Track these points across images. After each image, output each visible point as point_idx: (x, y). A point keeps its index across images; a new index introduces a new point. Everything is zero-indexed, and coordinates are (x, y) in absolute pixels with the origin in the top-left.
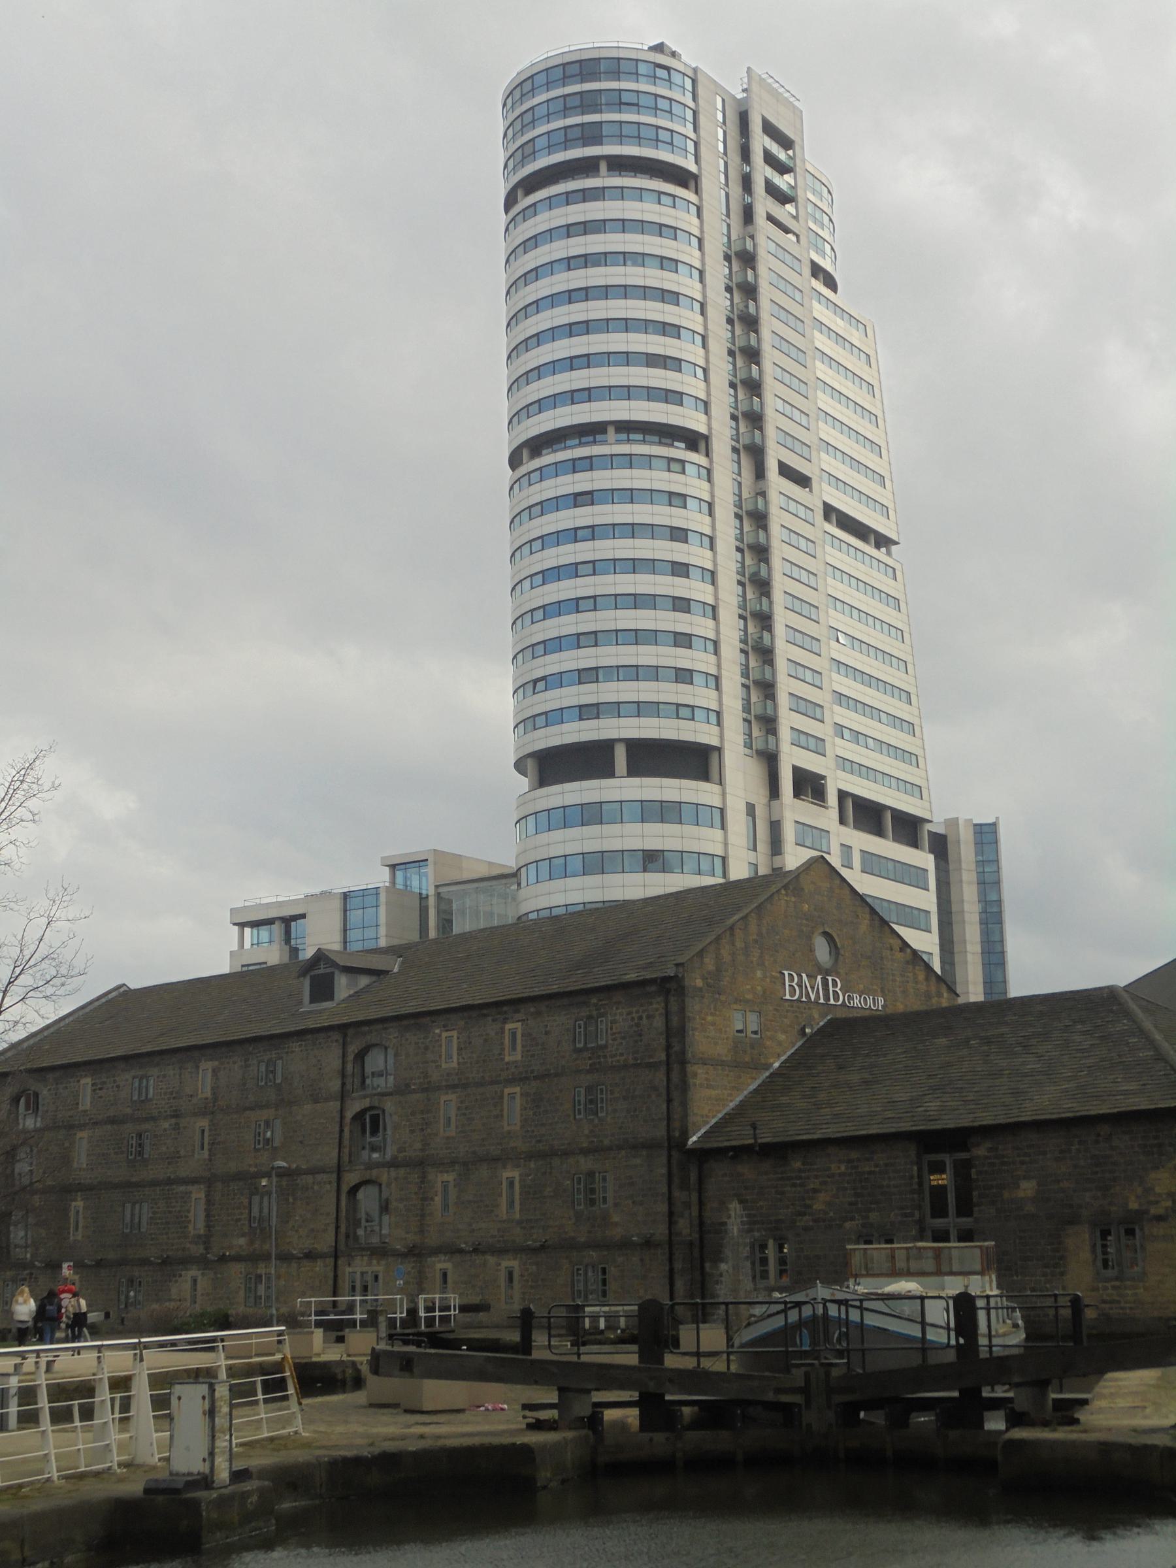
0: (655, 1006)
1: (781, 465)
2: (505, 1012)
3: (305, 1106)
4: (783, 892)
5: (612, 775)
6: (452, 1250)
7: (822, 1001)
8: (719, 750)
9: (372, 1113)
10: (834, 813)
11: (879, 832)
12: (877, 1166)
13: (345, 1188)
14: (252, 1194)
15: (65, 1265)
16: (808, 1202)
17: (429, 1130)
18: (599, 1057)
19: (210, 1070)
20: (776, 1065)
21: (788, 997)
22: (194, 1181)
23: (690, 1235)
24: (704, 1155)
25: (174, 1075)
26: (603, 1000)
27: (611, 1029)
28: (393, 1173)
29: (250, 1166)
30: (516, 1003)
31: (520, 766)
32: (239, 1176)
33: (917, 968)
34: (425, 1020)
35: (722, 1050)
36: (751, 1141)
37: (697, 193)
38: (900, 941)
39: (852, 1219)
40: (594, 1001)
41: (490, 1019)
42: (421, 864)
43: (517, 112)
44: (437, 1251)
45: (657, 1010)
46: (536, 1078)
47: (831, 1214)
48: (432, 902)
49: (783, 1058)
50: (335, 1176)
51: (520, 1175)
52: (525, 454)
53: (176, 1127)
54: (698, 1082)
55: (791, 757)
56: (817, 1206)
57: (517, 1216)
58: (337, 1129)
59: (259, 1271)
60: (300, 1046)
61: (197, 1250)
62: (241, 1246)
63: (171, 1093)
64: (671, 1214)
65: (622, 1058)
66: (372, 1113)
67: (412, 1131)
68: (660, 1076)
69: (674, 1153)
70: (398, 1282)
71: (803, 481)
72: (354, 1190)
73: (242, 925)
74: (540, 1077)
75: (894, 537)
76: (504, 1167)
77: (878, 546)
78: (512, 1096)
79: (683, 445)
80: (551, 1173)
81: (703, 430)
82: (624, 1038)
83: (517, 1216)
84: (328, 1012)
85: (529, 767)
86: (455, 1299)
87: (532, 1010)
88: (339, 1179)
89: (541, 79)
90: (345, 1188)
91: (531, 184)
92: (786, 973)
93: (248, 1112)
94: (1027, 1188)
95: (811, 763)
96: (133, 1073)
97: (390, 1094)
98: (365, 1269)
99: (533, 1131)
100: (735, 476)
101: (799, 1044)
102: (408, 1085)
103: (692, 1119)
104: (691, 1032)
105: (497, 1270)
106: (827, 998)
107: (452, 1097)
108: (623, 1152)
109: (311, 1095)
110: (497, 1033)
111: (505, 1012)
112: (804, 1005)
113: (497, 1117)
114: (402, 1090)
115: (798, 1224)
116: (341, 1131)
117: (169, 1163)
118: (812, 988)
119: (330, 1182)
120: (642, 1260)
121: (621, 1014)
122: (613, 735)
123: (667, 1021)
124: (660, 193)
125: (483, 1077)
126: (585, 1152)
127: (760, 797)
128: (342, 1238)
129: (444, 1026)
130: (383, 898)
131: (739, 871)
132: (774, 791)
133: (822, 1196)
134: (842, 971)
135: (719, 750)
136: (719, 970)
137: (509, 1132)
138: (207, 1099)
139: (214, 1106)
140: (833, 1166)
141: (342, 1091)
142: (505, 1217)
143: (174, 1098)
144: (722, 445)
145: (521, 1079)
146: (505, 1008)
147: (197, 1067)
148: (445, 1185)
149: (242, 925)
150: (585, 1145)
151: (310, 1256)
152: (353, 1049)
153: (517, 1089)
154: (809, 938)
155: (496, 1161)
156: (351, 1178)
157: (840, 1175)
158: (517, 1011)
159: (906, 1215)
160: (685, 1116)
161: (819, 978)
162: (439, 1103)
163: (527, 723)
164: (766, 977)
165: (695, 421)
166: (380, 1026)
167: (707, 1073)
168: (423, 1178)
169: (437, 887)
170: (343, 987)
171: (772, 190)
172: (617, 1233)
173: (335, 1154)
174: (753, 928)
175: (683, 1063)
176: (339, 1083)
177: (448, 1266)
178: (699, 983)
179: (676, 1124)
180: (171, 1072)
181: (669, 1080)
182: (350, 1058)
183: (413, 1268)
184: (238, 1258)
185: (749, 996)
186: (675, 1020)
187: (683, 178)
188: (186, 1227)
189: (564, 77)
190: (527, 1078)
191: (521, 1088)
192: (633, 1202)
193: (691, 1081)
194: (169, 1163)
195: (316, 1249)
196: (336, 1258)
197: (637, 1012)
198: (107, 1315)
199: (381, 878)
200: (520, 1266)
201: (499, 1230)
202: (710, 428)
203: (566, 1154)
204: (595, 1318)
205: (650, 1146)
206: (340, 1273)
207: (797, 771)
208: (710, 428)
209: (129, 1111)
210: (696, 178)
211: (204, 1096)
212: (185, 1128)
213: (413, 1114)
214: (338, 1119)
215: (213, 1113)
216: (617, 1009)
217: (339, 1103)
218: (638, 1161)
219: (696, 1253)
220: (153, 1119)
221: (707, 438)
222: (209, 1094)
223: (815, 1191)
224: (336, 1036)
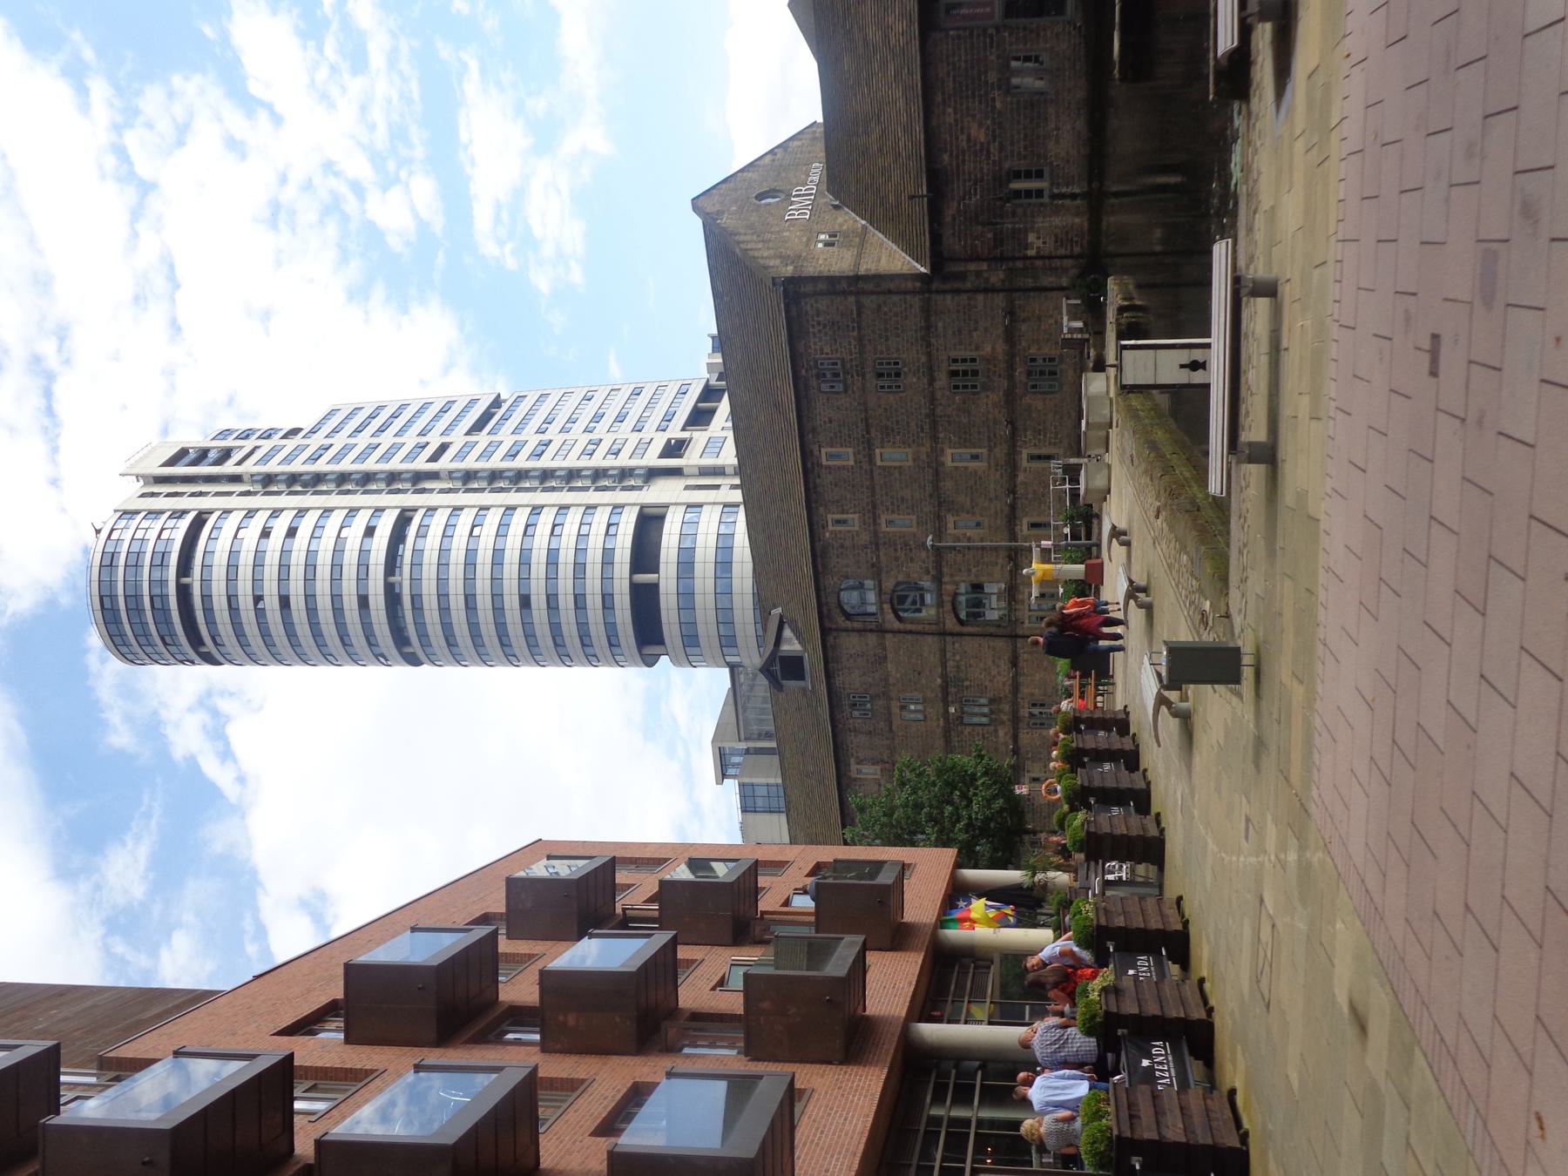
0: (809, 308)
1: (429, 460)
7: (812, 197)
8: (643, 507)
9: (896, 602)
10: (696, 435)
12: (948, 74)
14: (962, 723)
16: (978, 147)
18: (852, 366)
21: (807, 217)
24: (938, 259)
27: (827, 354)
28: (946, 579)
30: (806, 454)
36: (925, 199)
37: (212, 513)
39: (994, 100)
41: (818, 481)
43: (139, 650)
45: (812, 306)
46: (868, 433)
47: (989, 122)
48: (752, 744)
49: (858, 218)
50: (948, 638)
51: (950, 448)
52: (408, 650)
55: (652, 459)
56: (982, 138)
57: (984, 451)
58: (909, 637)
59: (1027, 715)
60: (838, 676)
62: (1006, 734)
64: (986, 290)
66: (896, 602)
67: (912, 560)
68: (868, 301)
69: (934, 286)
75: (494, 396)
76: (943, 464)
77: (499, 407)
79: (401, 546)
80: (949, 416)
82: (836, 340)
83: (984, 451)
84: (813, 662)
87: (810, 436)
88: (952, 634)
89: (113, 627)
90: (958, 628)
97: (880, 584)
101: (847, 209)
102: (873, 565)
103: (905, 270)
106: (811, 194)
107: (883, 519)
108: (933, 341)
110: (830, 473)
111: (813, 464)
113: (900, 474)
114: (876, 571)
115: (997, 158)
119: (954, 643)
120: (1024, 321)
121: (815, 344)
122: (626, 583)
123: (822, 293)
124: (209, 538)
125: (867, 488)
126: (932, 381)
129: (823, 528)
130: (746, 780)
131: (737, 496)
132: (676, 472)
133: (973, 132)
134: (788, 187)
136: (780, 257)
137: (914, 460)
138: (882, 770)
141: (878, 631)
142: (985, 464)
146: (809, 465)
147: (855, 780)
150: (926, 381)
152: (842, 622)
155: (937, 472)
157: (955, 113)
158: (811, 451)
159: (992, 43)
162: (888, 533)
166: (823, 594)
169: (740, 740)
170: (791, 646)
172: (1001, 347)
173: (929, 639)
176: (869, 635)
177: (1025, 521)
178: (790, 268)
179: (910, 285)
181: (873, 293)
182: (848, 624)
184: (1015, 738)
193: (873, 272)
197: (813, 326)
199: (732, 785)
201: (997, 470)
202: (396, 507)
203: (933, 399)
204: (1071, 330)
205: (927, 311)
207: (662, 456)
211: (879, 772)
213: (897, 559)
218: (940, 324)
222: (878, 768)
223: (969, 140)
224: (831, 639)
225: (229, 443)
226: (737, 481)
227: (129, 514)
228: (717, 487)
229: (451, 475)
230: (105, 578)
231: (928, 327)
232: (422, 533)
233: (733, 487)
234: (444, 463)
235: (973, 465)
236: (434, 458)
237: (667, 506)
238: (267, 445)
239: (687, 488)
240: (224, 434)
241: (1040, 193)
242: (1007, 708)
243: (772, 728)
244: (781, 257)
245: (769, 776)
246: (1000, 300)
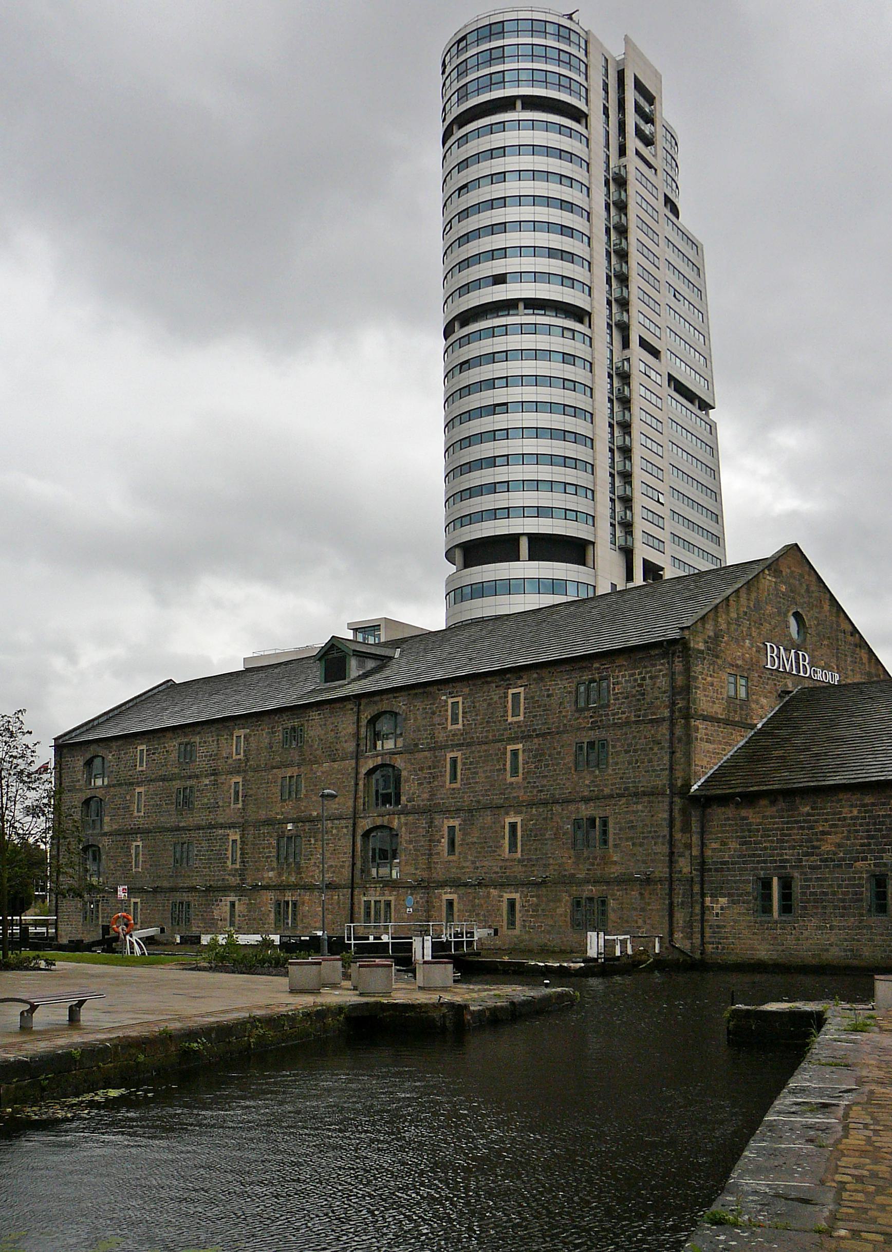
2: (509, 679)
3: (324, 765)
4: (767, 572)
6: (456, 884)
8: (593, 543)
13: (360, 832)
15: (120, 889)
17: (436, 783)
19: (243, 737)
20: (759, 726)
21: (769, 666)
22: (232, 826)
23: (691, 873)
25: (213, 741)
26: (605, 664)
29: (277, 814)
31: (449, 555)
32: (269, 822)
33: (863, 651)
34: (433, 689)
35: (717, 709)
38: (851, 627)
40: (596, 665)
42: (376, 628)
44: (442, 885)
48: (377, 851)
53: (215, 783)
54: (699, 736)
55: (642, 553)
56: (825, 847)
61: (234, 881)
62: (270, 878)
63: (211, 755)
64: (672, 854)
65: (624, 716)
67: (420, 784)
69: (677, 800)
70: (408, 910)
71: (655, 353)
74: (543, 735)
75: (713, 405)
76: (507, 814)
78: (515, 753)
85: (457, 556)
86: (624, 942)
87: (535, 675)
90: (360, 832)
91: (464, 119)
92: (768, 644)
93: (274, 770)
95: (656, 558)
96: (179, 740)
98: (378, 899)
99: (535, 782)
100: (609, 345)
102: (416, 745)
104: (694, 690)
105: (499, 901)
109: (330, 755)
112: (780, 674)
116: (357, 784)
117: (210, 812)
118: (788, 660)
119: (347, 827)
120: (641, 894)
126: (586, 800)
128: (358, 873)
133: (832, 838)
135: (593, 543)
136: (717, 636)
137: (512, 784)
139: (246, 765)
140: (845, 810)
143: (213, 760)
145: (523, 738)
148: (452, 829)
151: (330, 886)
152: (365, 717)
153: (520, 746)
154: (786, 615)
155: (498, 809)
157: (852, 818)
158: (520, 678)
161: (793, 651)
163: (455, 523)
164: (753, 647)
167: (706, 729)
168: (431, 824)
170: (354, 668)
171: (639, 133)
172: (615, 871)
173: (350, 803)
174: (743, 600)
175: (687, 717)
177: (454, 897)
178: (701, 646)
179: (679, 774)
180: (210, 739)
181: (672, 734)
182: (364, 722)
183: (421, 898)
184: (266, 888)
185: (740, 662)
187: (578, 115)
188: (225, 863)
189: (491, 35)
190: (530, 736)
191: (523, 746)
192: (633, 844)
194: (210, 812)
195: (335, 881)
196: (353, 888)
198: (162, 930)
200: (521, 898)
201: (501, 867)
206: (356, 901)
208: (592, 308)
209: (176, 771)
212: (222, 783)
214: (353, 775)
215: (245, 771)
216: (620, 671)
217: (353, 762)
219: (697, 889)
220: (197, 777)
223: (823, 833)
225: (660, 141)
244: (717, 637)
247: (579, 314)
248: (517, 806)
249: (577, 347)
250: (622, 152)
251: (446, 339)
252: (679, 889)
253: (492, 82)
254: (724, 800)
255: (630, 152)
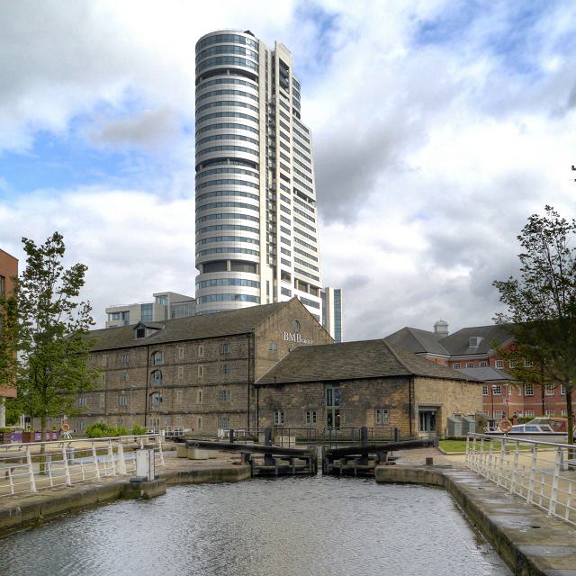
5: (226, 270)
11: (306, 291)
24: (258, 387)
32: (115, 390)
35: (265, 355)
48: (169, 308)
52: (201, 167)
55: (281, 267)
61: (102, 412)
72: (151, 395)
73: (109, 313)
81: (257, 161)
84: (143, 341)
94: (356, 398)
95: (286, 268)
127: (270, 278)
131: (264, 302)
144: (263, 167)
149: (109, 313)
152: (150, 353)
156: (150, 391)
160: (254, 374)
165: (253, 158)
170: (148, 333)
175: (253, 358)
184: (115, 415)
186: (251, 346)
199: (152, 300)
210: (258, 78)
221: (258, 165)
225: (291, 86)
226: (271, 302)
227: (257, 46)
228: (268, 294)
229: (274, 184)
230: (236, 38)
231: (239, 384)
232: (248, 173)
233: (268, 300)
234: (280, 181)
235: (198, 399)
236: (282, 176)
237: (259, 274)
238: (290, 104)
239: (268, 282)
240: (297, 84)
241: (277, 422)
242: (124, 411)
243: (176, 317)
244: (265, 332)
245: (156, 317)
246: (246, 408)
247: (254, 165)
248: (201, 386)
249: (253, 179)
250: (274, 91)
251: (197, 171)
252: (251, 415)
253: (219, 61)
254: (264, 386)
255: (277, 93)
